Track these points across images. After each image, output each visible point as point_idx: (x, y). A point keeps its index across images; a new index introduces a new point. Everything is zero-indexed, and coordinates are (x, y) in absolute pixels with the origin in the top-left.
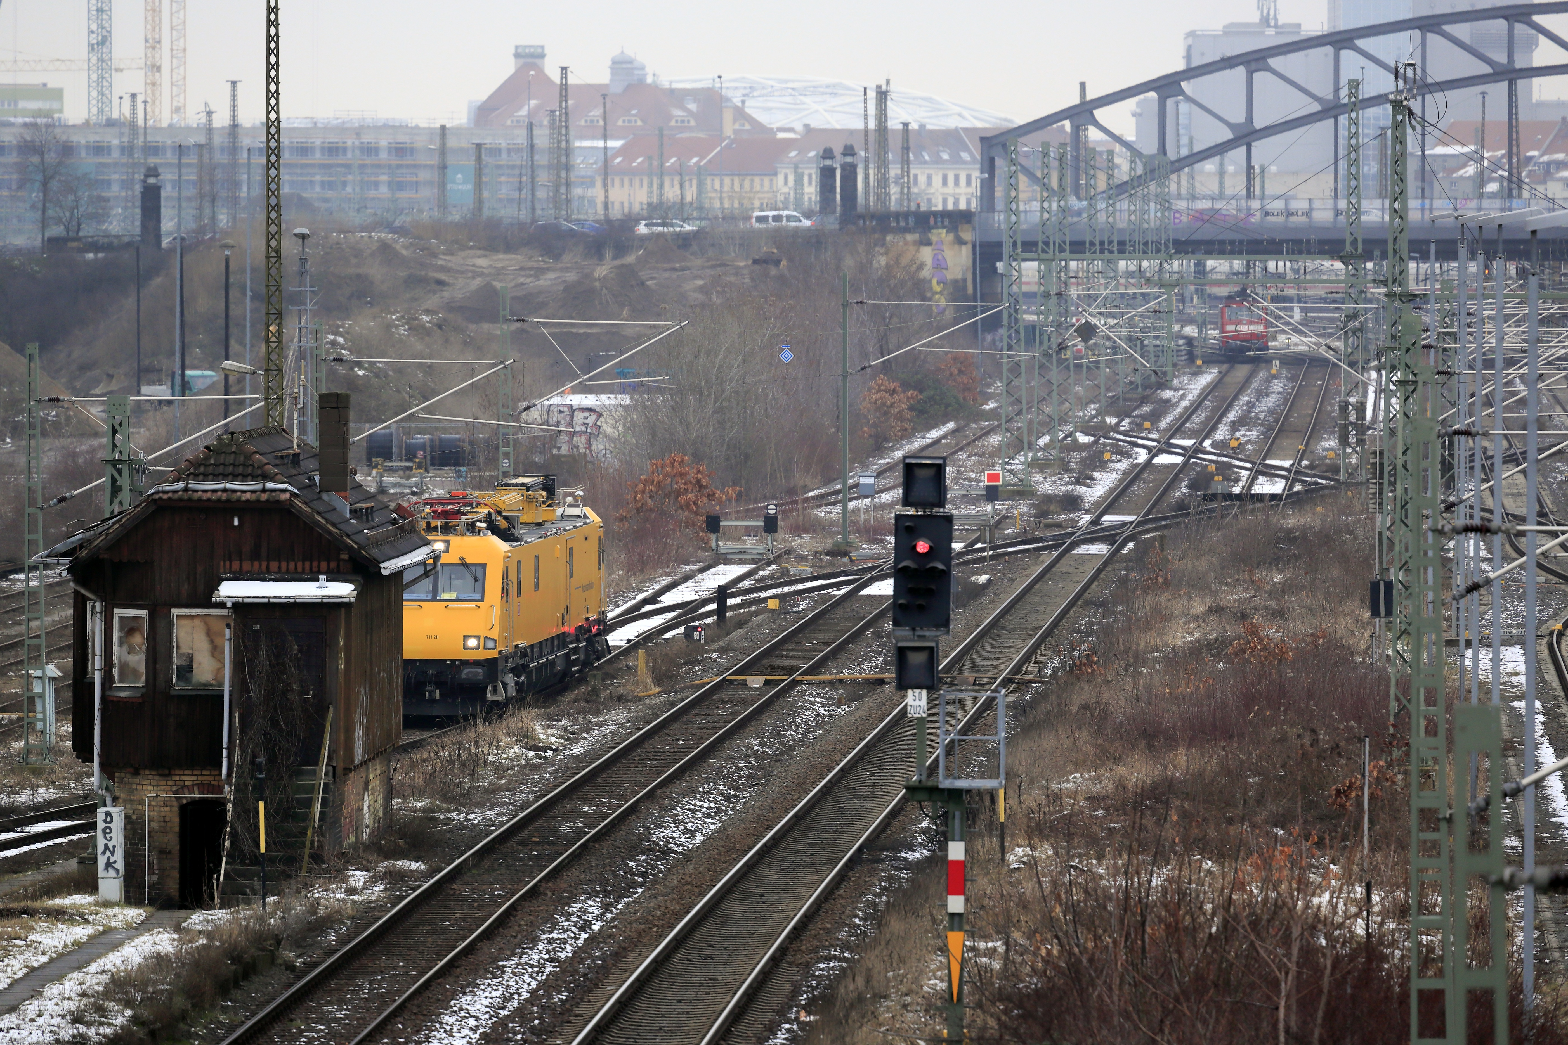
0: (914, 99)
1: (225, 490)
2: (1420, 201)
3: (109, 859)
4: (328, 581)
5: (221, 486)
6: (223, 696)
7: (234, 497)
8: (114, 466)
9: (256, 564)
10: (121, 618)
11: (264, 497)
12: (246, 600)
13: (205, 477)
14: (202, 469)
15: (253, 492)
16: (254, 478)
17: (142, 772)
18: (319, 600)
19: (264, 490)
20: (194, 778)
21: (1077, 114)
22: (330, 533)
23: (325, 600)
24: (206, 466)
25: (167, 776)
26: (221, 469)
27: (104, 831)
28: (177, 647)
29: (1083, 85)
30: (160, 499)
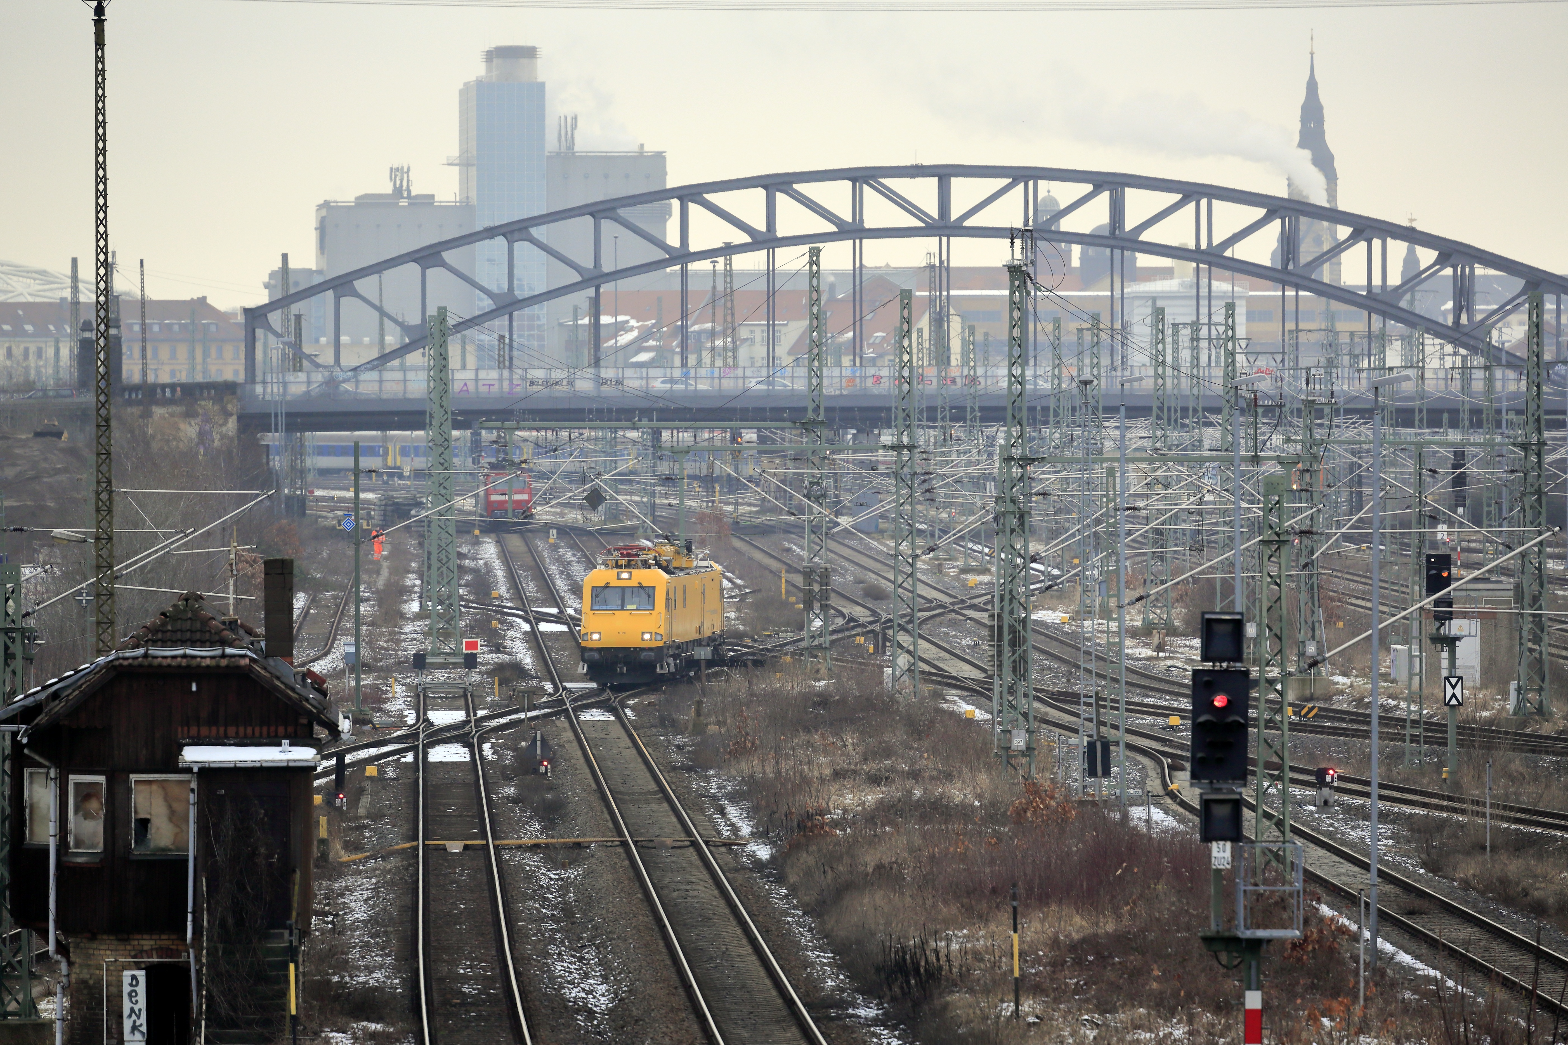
0: (32, 272)
1: (185, 656)
2: (592, 370)
3: (135, 1022)
4: (290, 745)
5: (181, 652)
6: (187, 860)
7: (194, 663)
8: (6, 634)
9: (214, 729)
10: (77, 785)
11: (224, 662)
12: (212, 765)
13: (164, 643)
14: (160, 635)
15: (212, 657)
16: (212, 644)
17: (99, 937)
18: (285, 764)
19: (223, 656)
20: (152, 942)
21: (341, 284)
22: (289, 698)
23: (291, 764)
24: (164, 632)
25: (126, 941)
26: (179, 635)
27: (130, 995)
28: (136, 812)
29: (285, 257)
30: (121, 665)
